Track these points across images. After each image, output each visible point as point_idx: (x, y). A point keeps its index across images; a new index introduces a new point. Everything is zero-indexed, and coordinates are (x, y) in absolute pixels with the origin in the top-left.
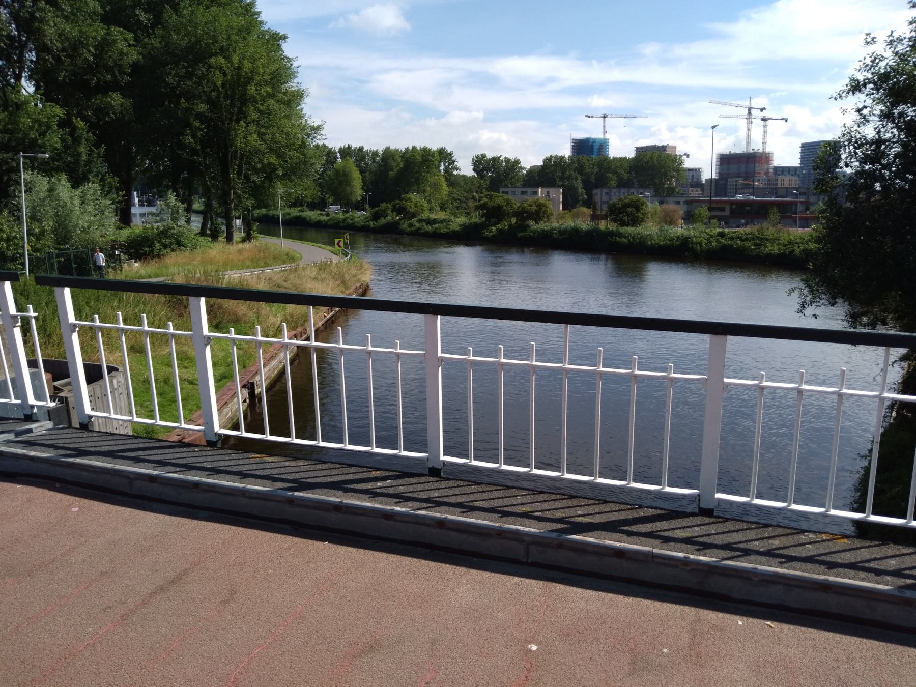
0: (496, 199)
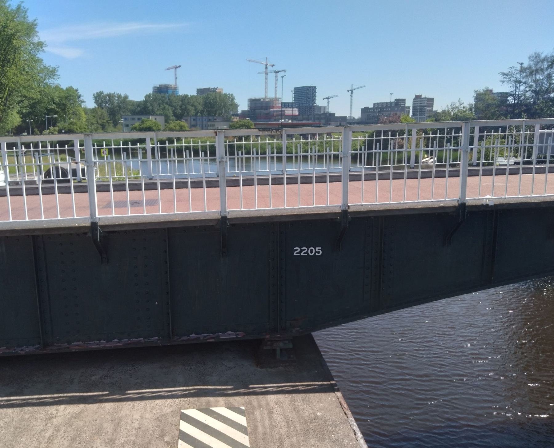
0: (147, 122)
